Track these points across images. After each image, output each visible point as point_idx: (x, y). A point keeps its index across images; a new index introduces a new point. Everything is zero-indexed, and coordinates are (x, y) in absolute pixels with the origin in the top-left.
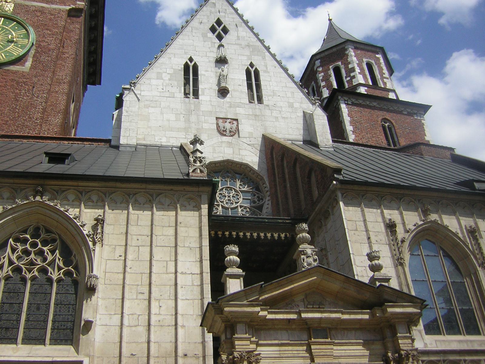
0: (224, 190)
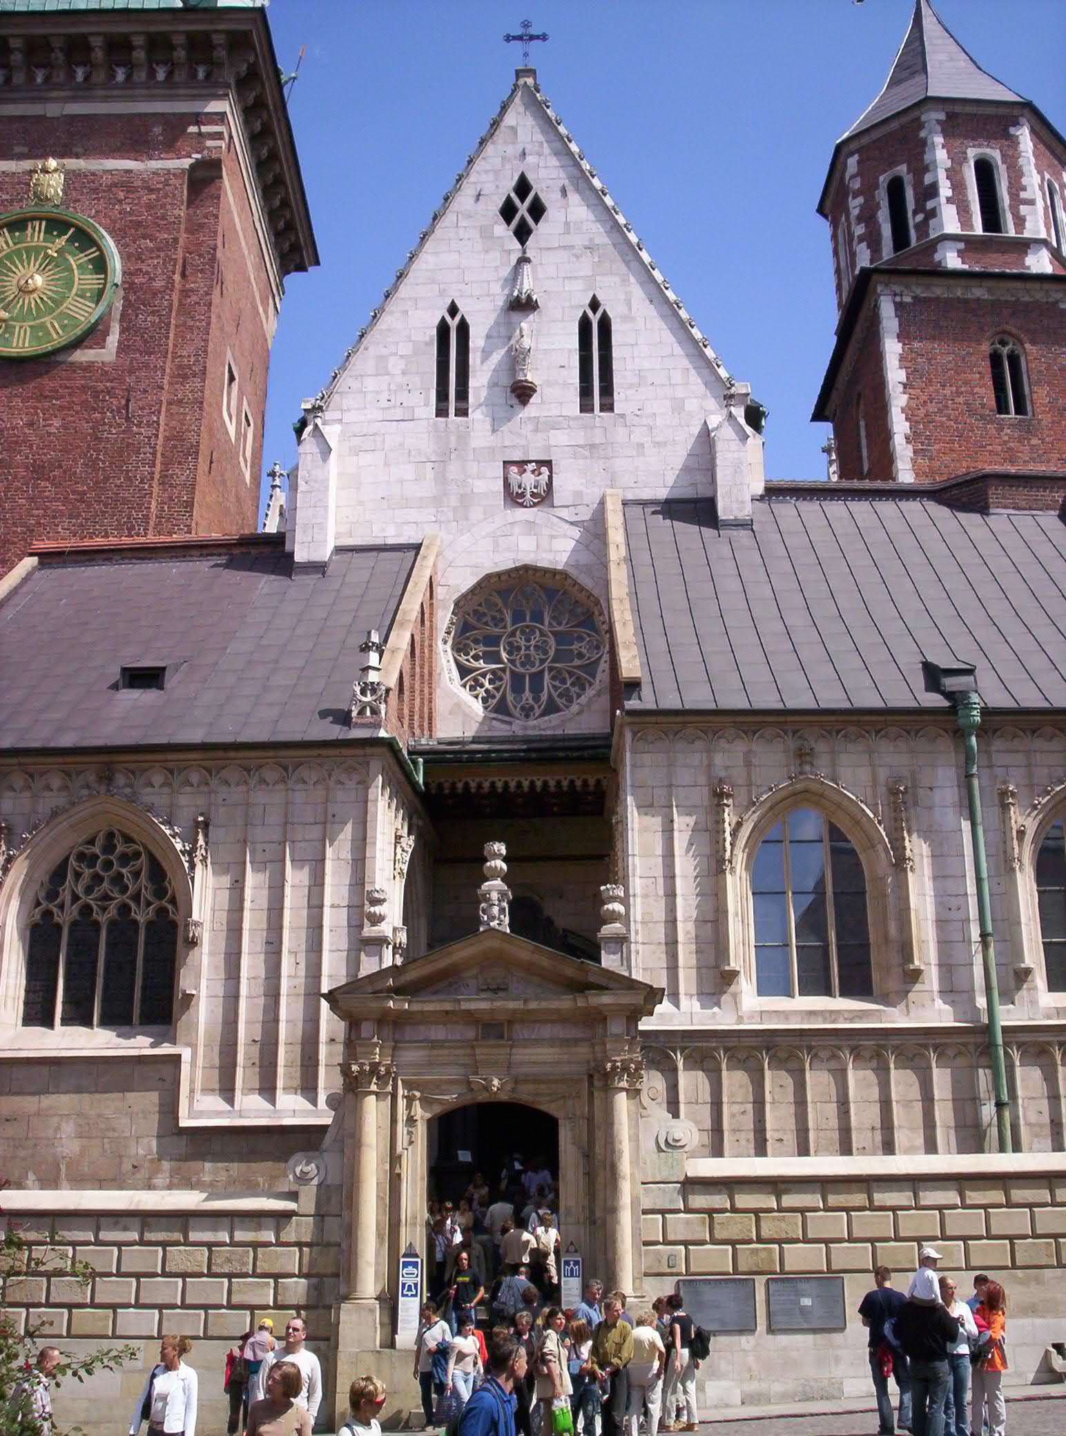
0: (518, 633)
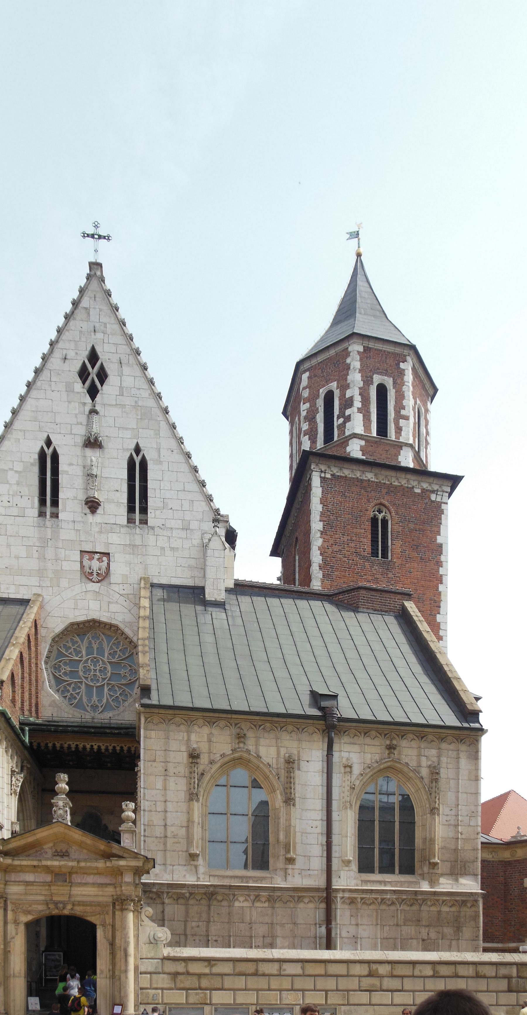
0: (89, 661)
